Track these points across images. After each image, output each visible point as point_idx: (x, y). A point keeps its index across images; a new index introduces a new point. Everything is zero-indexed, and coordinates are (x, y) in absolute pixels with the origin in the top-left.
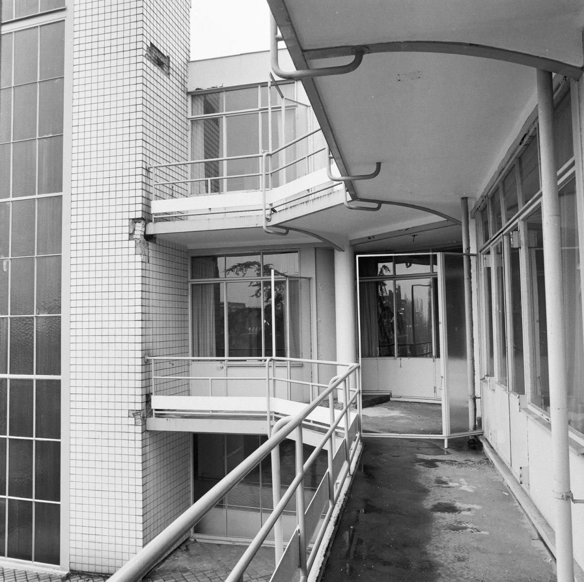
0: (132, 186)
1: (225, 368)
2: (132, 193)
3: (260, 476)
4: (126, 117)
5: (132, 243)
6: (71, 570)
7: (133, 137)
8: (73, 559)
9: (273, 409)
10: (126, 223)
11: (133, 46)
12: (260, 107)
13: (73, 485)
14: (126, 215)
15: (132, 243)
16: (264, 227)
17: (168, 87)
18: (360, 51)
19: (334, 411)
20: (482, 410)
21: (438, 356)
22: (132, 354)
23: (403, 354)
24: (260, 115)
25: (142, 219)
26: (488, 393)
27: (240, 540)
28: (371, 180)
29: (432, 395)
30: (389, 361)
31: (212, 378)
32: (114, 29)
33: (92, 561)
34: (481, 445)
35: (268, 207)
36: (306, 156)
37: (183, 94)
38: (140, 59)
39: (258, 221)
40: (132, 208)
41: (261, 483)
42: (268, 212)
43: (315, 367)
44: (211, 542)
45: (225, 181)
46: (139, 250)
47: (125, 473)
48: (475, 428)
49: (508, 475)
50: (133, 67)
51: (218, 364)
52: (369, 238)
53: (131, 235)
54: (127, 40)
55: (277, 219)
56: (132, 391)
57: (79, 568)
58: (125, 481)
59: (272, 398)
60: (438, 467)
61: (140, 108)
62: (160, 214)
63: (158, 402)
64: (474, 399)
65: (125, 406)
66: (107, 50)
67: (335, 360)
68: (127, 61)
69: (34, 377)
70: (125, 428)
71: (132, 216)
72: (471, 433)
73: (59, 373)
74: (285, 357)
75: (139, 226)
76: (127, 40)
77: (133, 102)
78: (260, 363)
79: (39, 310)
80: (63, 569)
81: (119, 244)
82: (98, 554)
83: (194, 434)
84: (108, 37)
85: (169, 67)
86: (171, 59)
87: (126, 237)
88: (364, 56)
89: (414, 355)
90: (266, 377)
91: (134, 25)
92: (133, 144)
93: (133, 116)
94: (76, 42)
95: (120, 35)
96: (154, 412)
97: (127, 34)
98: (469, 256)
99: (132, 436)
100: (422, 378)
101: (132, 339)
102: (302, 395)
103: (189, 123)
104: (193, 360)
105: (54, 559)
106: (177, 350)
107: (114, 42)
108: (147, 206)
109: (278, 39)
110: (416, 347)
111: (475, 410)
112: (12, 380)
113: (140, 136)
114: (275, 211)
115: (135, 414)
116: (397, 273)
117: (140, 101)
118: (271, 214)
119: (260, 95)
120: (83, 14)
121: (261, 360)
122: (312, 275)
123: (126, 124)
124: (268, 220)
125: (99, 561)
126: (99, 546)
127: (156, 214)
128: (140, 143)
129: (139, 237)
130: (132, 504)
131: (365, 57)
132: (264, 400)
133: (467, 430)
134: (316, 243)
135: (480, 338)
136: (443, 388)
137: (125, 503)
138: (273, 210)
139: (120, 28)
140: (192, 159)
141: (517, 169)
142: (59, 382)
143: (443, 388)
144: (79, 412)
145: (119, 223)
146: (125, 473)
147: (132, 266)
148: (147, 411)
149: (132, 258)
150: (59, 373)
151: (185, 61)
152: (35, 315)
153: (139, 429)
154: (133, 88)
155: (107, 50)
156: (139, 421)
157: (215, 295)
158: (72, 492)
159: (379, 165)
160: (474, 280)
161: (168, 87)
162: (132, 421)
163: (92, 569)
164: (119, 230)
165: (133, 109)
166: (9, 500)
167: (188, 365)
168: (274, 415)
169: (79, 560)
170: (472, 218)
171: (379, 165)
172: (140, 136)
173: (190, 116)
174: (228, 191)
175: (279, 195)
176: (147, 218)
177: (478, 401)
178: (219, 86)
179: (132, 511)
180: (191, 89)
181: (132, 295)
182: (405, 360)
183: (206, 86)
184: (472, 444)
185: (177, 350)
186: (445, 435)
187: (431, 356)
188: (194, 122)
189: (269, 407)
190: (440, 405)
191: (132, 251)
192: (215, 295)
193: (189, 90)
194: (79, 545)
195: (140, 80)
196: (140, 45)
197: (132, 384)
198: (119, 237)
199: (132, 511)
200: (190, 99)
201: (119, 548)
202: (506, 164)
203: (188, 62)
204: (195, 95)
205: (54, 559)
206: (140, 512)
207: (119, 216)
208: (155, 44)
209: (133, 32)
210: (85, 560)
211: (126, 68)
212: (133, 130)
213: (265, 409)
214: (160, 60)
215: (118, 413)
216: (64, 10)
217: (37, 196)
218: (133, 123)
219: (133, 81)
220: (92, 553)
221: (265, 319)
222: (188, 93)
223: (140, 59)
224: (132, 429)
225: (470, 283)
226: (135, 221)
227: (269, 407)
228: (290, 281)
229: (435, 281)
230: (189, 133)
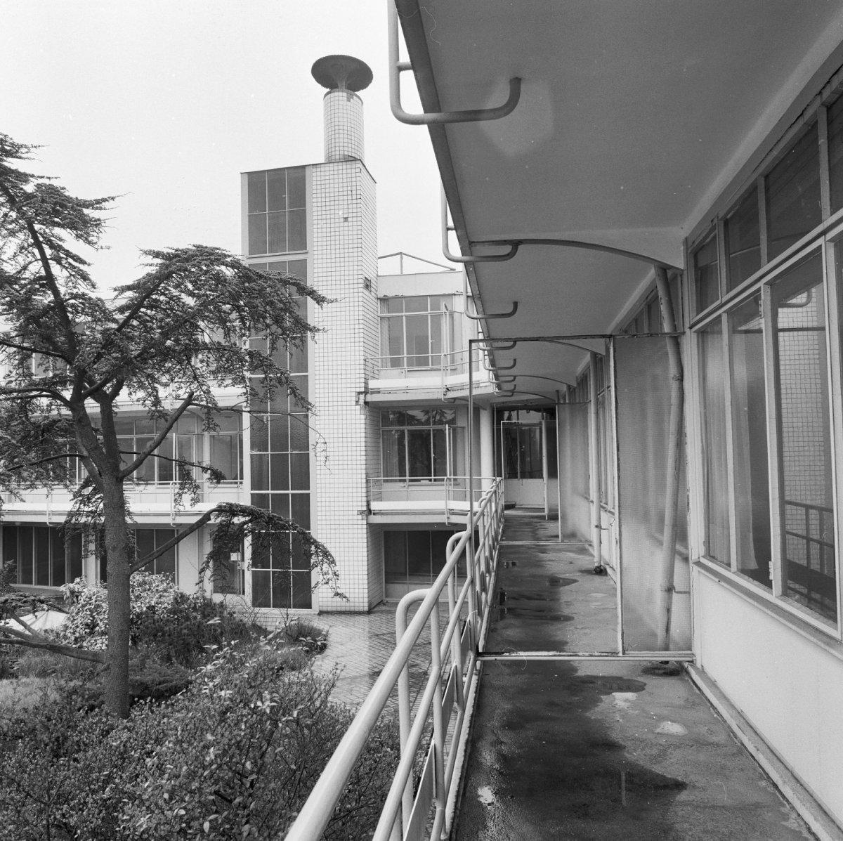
4: (352, 327)
7: (357, 340)
8: (321, 604)
10: (354, 394)
14: (353, 390)
15: (358, 407)
18: (515, 341)
22: (359, 476)
23: (523, 477)
28: (517, 313)
30: (515, 481)
32: (343, 269)
39: (439, 395)
40: (358, 385)
45: (405, 359)
47: (356, 550)
51: (402, 484)
55: (451, 395)
57: (325, 609)
60: (679, 786)
61: (361, 321)
63: (375, 506)
67: (480, 475)
69: (290, 492)
70: (355, 522)
71: (358, 390)
75: (362, 397)
76: (351, 277)
79: (293, 449)
81: (349, 408)
84: (338, 273)
87: (354, 403)
89: (532, 477)
92: (357, 344)
101: (359, 467)
102: (460, 498)
104: (387, 481)
109: (401, 69)
112: (273, 495)
115: (362, 513)
116: (781, 334)
117: (361, 317)
131: (520, 247)
141: (645, 317)
147: (358, 421)
149: (358, 417)
153: (365, 522)
156: (365, 517)
157: (411, 440)
161: (371, 297)
162: (360, 517)
180: (381, 295)
182: (524, 480)
183: (390, 294)
191: (358, 412)
192: (411, 440)
196: (360, 276)
198: (349, 404)
204: (384, 300)
207: (349, 390)
212: (357, 335)
215: (350, 513)
224: (360, 522)
226: (360, 393)
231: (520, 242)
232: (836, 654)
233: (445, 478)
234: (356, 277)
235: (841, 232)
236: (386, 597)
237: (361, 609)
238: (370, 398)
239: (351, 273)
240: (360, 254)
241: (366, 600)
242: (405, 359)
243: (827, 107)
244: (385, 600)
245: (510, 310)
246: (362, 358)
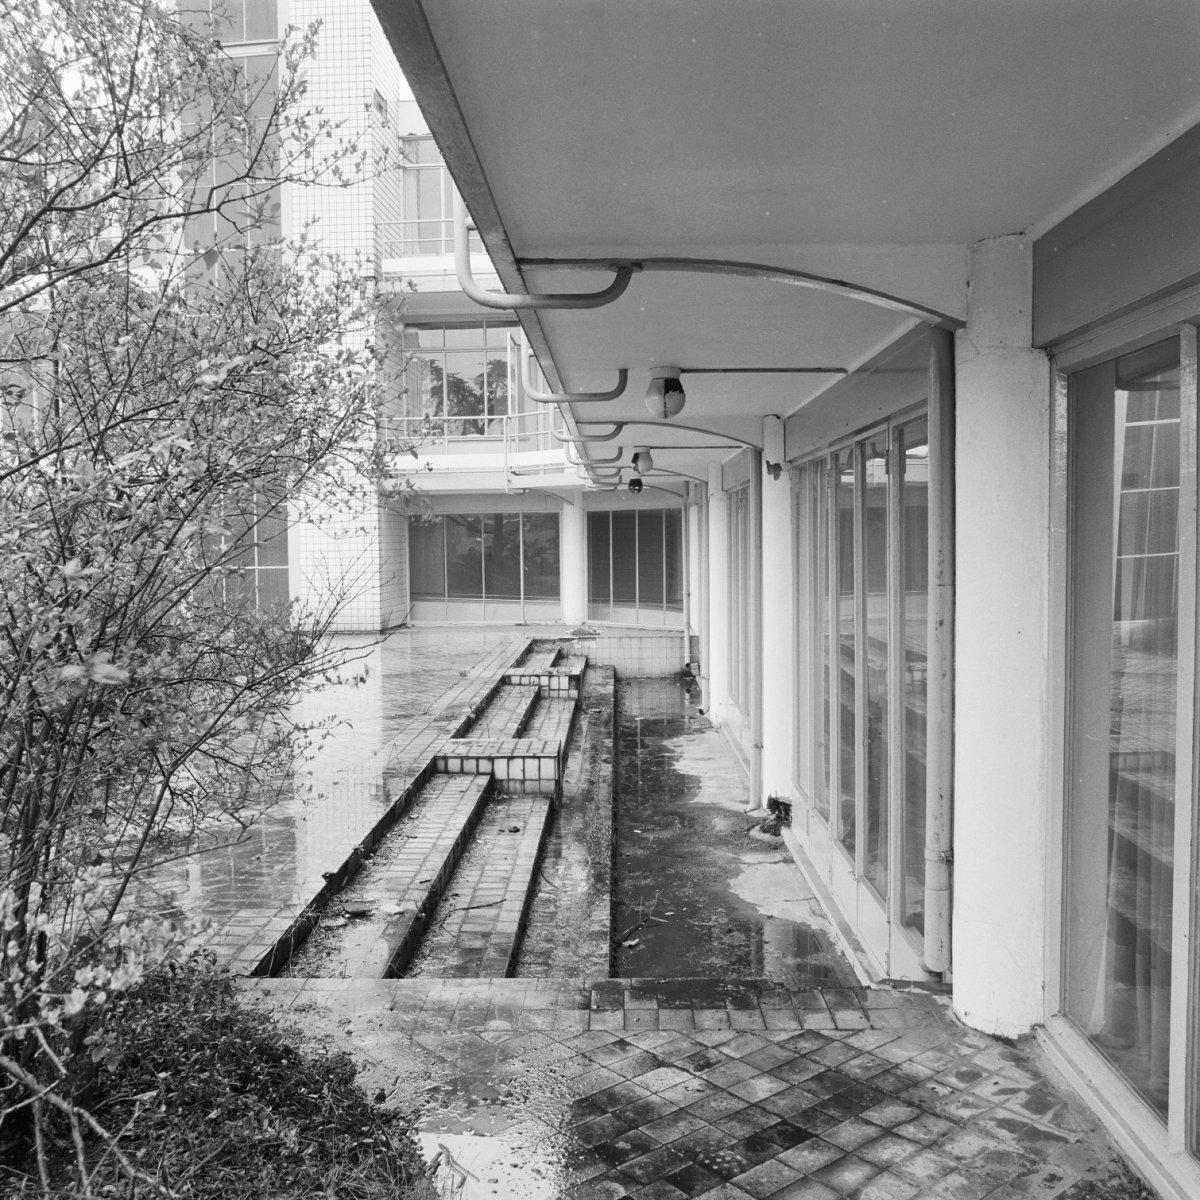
18: (625, 270)
19: (610, 423)
31: (818, 896)
41: (665, 604)
43: (541, 417)
45: (443, 243)
49: (1126, 873)
88: (335, 871)
131: (636, 277)
140: (405, 218)
159: (624, 373)
171: (624, 373)
180: (404, 133)
193: (400, 135)
222: (399, 138)
231: (639, 265)
232: (1113, 881)
233: (505, 417)
234: (361, 85)
235: (1192, 133)
236: (412, 618)
237: (370, 628)
238: (385, 287)
239: (353, 78)
240: (367, 62)
241: (378, 612)
242: (443, 243)
243: (1028, 1038)
244: (409, 622)
245: (613, 385)
246: (371, 220)
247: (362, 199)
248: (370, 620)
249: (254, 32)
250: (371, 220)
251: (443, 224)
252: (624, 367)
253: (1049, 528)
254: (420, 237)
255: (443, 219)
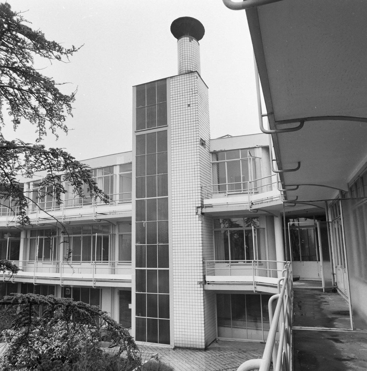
0: (197, 194)
1: (230, 266)
2: (197, 197)
3: (246, 313)
4: (193, 167)
5: (197, 216)
6: (175, 346)
7: (196, 175)
8: (176, 342)
9: (255, 281)
10: (195, 208)
11: (195, 140)
12: (241, 158)
13: (175, 312)
14: (194, 205)
15: (197, 216)
16: (249, 210)
17: (205, 151)
18: (302, 121)
20: (337, 278)
21: (319, 260)
23: (303, 260)
24: (241, 161)
25: (201, 207)
26: (339, 272)
27: (239, 339)
29: (318, 277)
30: (298, 263)
33: (184, 342)
34: (337, 291)
35: (250, 202)
36: (266, 185)
37: (208, 153)
38: (198, 145)
39: (247, 207)
40: (197, 202)
42: (250, 204)
44: (227, 340)
46: (200, 219)
47: (196, 307)
48: (334, 285)
50: (195, 148)
51: (227, 264)
52: (289, 212)
53: (197, 213)
54: (192, 138)
55: (254, 207)
56: (199, 274)
57: (178, 345)
58: (197, 310)
59: (255, 276)
61: (199, 164)
62: (207, 205)
63: (209, 278)
64: (334, 274)
65: (196, 280)
66: (185, 142)
68: (193, 146)
70: (196, 289)
71: (197, 206)
72: (333, 287)
73: (168, 267)
74: (130, 292)
75: (200, 210)
76: (192, 138)
77: (196, 162)
78: (244, 263)
79: (159, 242)
80: (172, 346)
81: (192, 217)
82: (186, 339)
83: (217, 295)
85: (205, 144)
86: (206, 141)
87: (195, 214)
90: (252, 268)
91: (195, 133)
93: (196, 167)
94: (172, 138)
95: (190, 136)
96: (207, 282)
97: (192, 136)
98: (329, 222)
99: (199, 292)
100: (314, 271)
102: (267, 274)
103: (211, 165)
105: (168, 342)
106: (211, 259)
107: (187, 139)
108: (202, 201)
110: (311, 257)
111: (334, 278)
113: (199, 175)
114: (253, 204)
117: (198, 161)
118: (251, 205)
119: (240, 152)
120: (175, 128)
121: (244, 262)
122: (265, 227)
123: (193, 170)
124: (250, 207)
125: (186, 343)
126: (186, 337)
127: (205, 205)
128: (199, 177)
129: (200, 214)
130: (200, 319)
131: (306, 123)
132: (252, 277)
133: (332, 285)
134: (269, 215)
135: (334, 252)
136: (322, 270)
137: (197, 319)
138: (252, 203)
139: (190, 133)
142: (168, 270)
143: (322, 270)
144: (177, 283)
145: (192, 208)
146: (196, 307)
148: (205, 282)
150: (168, 267)
151: (209, 139)
152: (157, 244)
153: (202, 289)
154: (196, 156)
155: (185, 142)
156: (202, 286)
157: (230, 237)
158: (175, 315)
159: (299, 163)
160: (331, 231)
161: (205, 151)
163: (184, 346)
164: (192, 211)
165: (196, 164)
166: (147, 319)
167: (214, 265)
168: (255, 283)
169: (178, 342)
170: (330, 207)
171: (299, 163)
172: (199, 175)
173: (211, 162)
174: (136, 136)
175: (255, 198)
176: (202, 207)
177: (335, 275)
178: (223, 149)
179: (200, 322)
180: (212, 150)
181: (198, 236)
183: (217, 150)
184: (333, 290)
185: (211, 259)
186: (323, 286)
187: (316, 261)
188: (213, 164)
189: (254, 280)
190: (321, 281)
191: (197, 219)
192: (230, 237)
193: (211, 151)
194: (178, 336)
195: (198, 153)
197: (199, 271)
198: (192, 214)
199: (200, 322)
200: (211, 155)
201: (195, 337)
202: (285, 323)
203: (210, 139)
205: (168, 342)
206: (203, 322)
208: (203, 139)
209: (195, 135)
210: (181, 342)
211: (193, 149)
213: (252, 281)
214: (203, 143)
216: (167, 126)
217: (157, 197)
218: (196, 170)
219: (195, 154)
220: (183, 339)
221: (246, 245)
222: (210, 153)
223: (198, 145)
224: (199, 289)
225: (330, 232)
226: (198, 207)
227: (254, 280)
228: (257, 230)
229: (317, 228)
230: (211, 168)
236: (218, 336)
237: (200, 347)
244: (218, 338)
247: (196, 178)
248: (200, 344)
249: (112, 172)
250: (199, 186)
251: (242, 184)
252: (299, 161)
253: (18, 183)
254: (219, 191)
255: (242, 182)
